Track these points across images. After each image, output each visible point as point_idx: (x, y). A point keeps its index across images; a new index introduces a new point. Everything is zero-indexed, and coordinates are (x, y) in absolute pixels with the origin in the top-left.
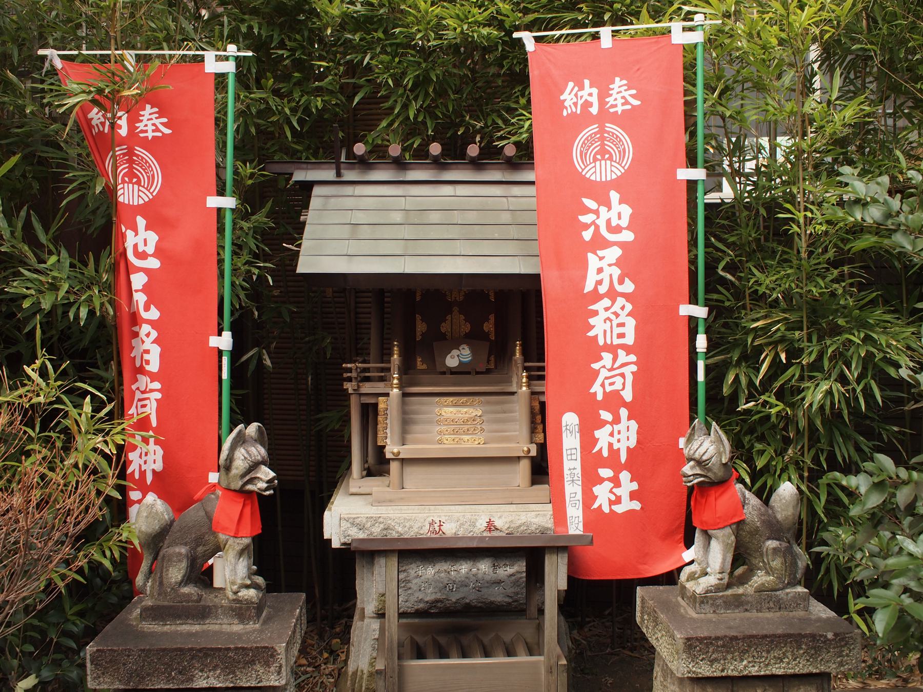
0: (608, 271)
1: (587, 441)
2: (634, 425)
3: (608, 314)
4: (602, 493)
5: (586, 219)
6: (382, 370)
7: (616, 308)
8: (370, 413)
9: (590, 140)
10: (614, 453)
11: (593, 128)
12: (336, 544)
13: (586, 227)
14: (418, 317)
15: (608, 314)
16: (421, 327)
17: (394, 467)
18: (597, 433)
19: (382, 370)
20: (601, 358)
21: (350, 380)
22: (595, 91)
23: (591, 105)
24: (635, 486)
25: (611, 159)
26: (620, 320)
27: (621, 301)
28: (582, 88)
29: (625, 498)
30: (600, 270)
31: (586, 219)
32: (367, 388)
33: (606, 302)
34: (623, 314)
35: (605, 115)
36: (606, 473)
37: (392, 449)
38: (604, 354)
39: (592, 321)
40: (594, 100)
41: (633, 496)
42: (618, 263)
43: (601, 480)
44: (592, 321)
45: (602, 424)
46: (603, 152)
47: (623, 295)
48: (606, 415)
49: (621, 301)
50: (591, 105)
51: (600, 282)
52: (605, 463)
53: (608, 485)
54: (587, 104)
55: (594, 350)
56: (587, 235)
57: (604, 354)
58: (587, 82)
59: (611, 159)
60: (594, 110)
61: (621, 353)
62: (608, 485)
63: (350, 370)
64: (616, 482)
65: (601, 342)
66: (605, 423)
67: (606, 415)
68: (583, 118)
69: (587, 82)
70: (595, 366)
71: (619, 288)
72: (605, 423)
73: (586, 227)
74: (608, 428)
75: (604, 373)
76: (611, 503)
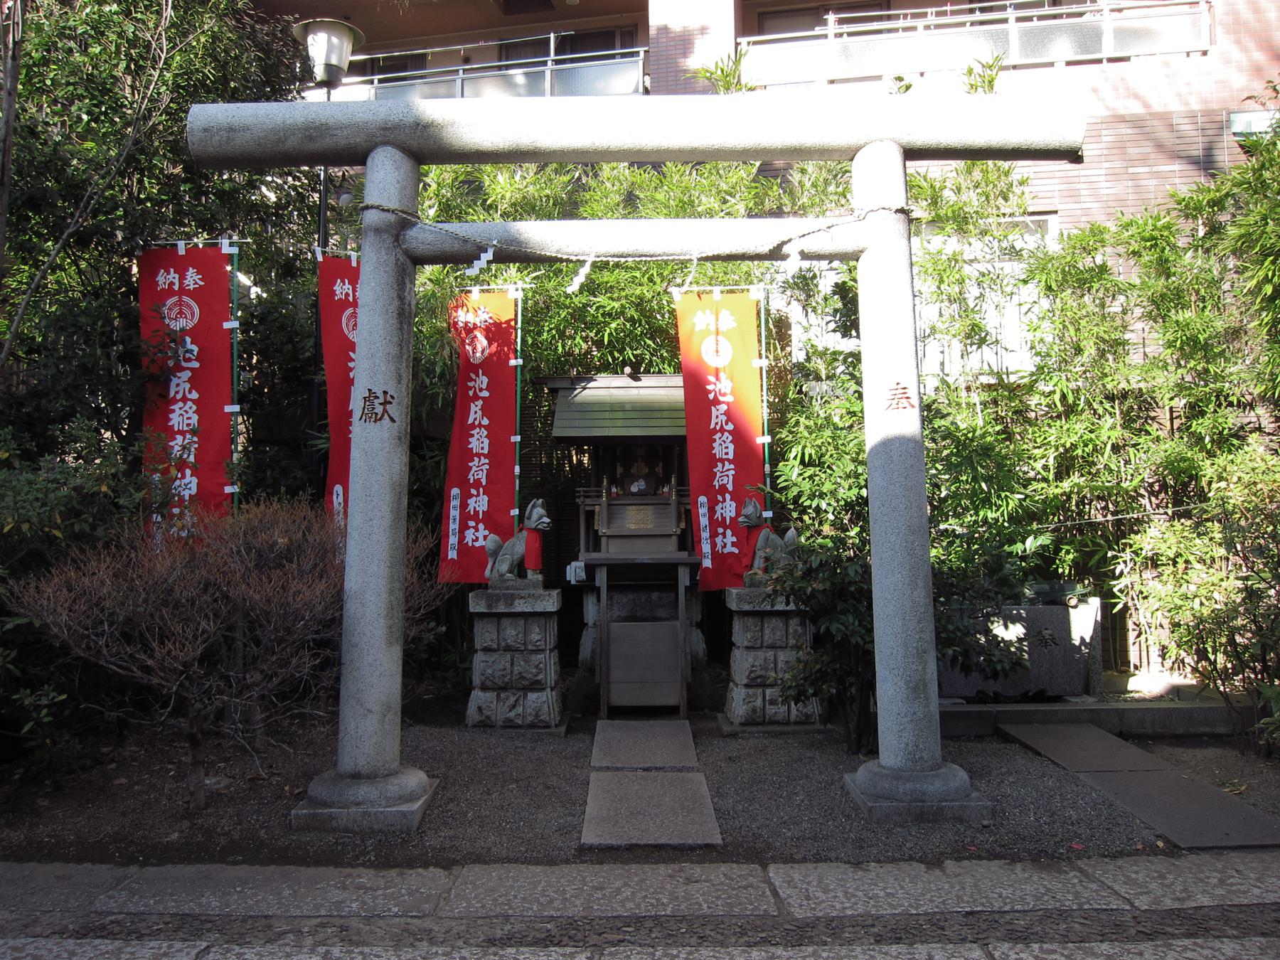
0: (183, 385)
1: (464, 505)
2: (486, 498)
3: (182, 412)
4: (470, 535)
5: (471, 384)
6: (598, 491)
7: (186, 408)
8: (590, 515)
9: (175, 304)
10: (476, 513)
11: (175, 299)
12: (573, 582)
13: (470, 388)
14: (618, 464)
15: (182, 412)
16: (620, 470)
17: (604, 540)
18: (469, 501)
19: (598, 491)
20: (175, 439)
21: (579, 497)
22: (177, 276)
23: (174, 284)
24: (734, 539)
25: (186, 317)
26: (188, 416)
27: (190, 404)
28: (169, 273)
29: (729, 545)
30: (178, 385)
31: (471, 384)
32: (588, 501)
33: (181, 404)
34: (191, 412)
35: (183, 291)
36: (472, 523)
37: (603, 530)
38: (177, 436)
39: (171, 416)
40: (177, 281)
41: (733, 544)
42: (190, 380)
43: (469, 528)
44: (171, 416)
45: (471, 496)
46: (181, 313)
47: (191, 400)
48: (474, 492)
49: (190, 404)
50: (174, 284)
51: (177, 392)
52: (471, 518)
53: (472, 530)
54: (172, 284)
55: (470, 455)
56: (471, 393)
57: (177, 436)
58: (172, 270)
59: (186, 317)
60: (176, 287)
61: (188, 436)
62: (472, 530)
63: (579, 492)
64: (724, 535)
65: (176, 429)
66: (473, 495)
67: (474, 492)
68: (170, 292)
69: (172, 270)
70: (470, 464)
71: (189, 396)
72: (473, 495)
73: (470, 388)
74: (474, 499)
75: (474, 469)
76: (473, 541)
